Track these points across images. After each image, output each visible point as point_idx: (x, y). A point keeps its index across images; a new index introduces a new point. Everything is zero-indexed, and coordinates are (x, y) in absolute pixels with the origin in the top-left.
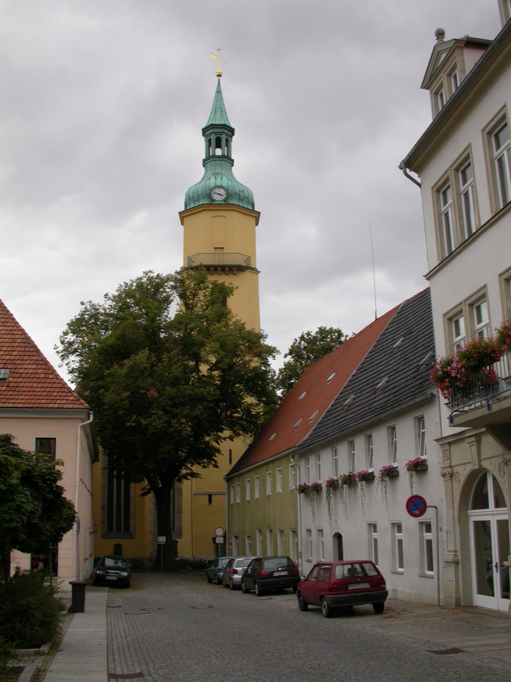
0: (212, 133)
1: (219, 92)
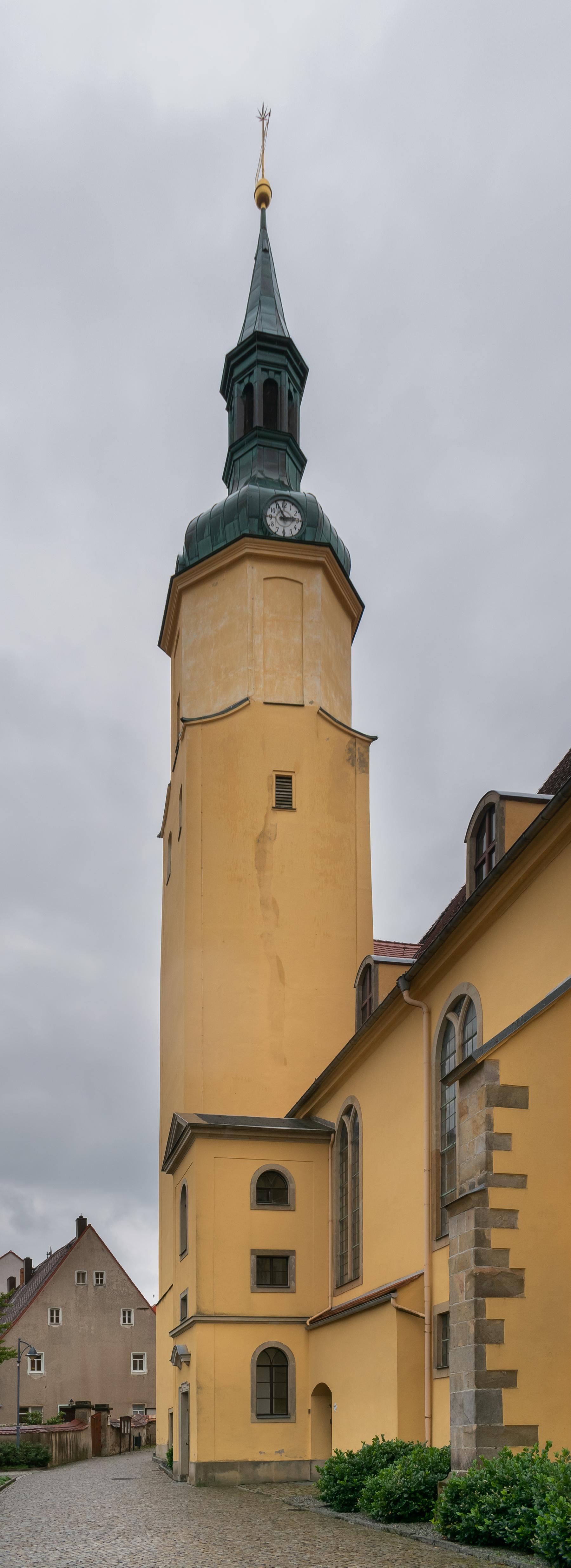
0: (258, 362)
1: (264, 252)
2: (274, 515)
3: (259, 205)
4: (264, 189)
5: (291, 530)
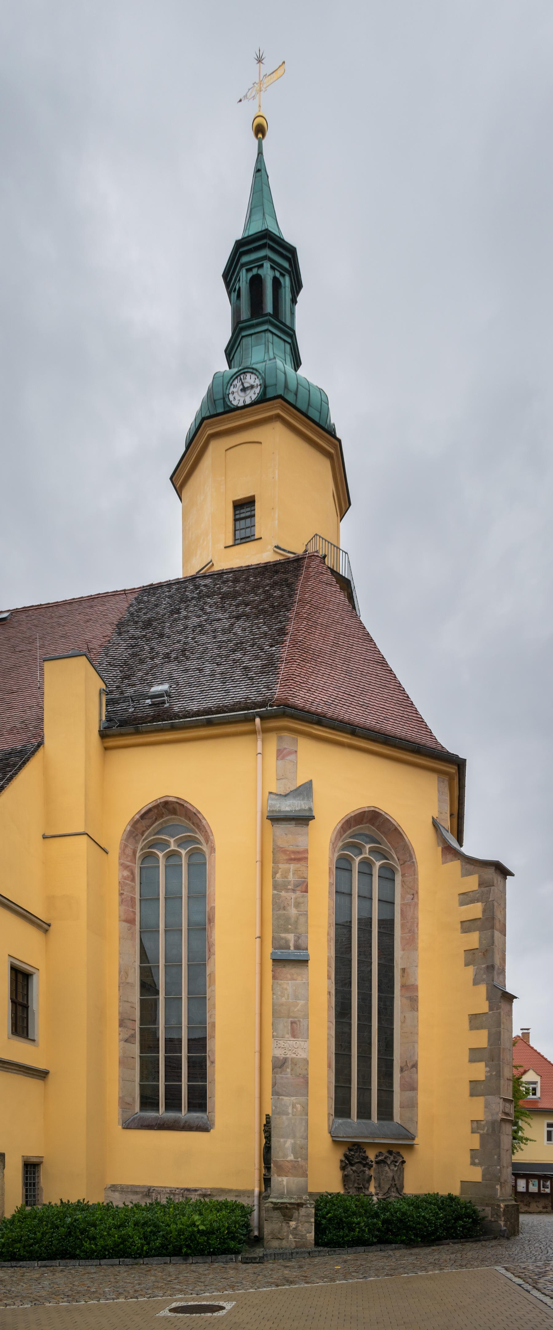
1: (260, 170)
2: (235, 390)
3: (256, 135)
4: (259, 120)
5: (252, 396)
